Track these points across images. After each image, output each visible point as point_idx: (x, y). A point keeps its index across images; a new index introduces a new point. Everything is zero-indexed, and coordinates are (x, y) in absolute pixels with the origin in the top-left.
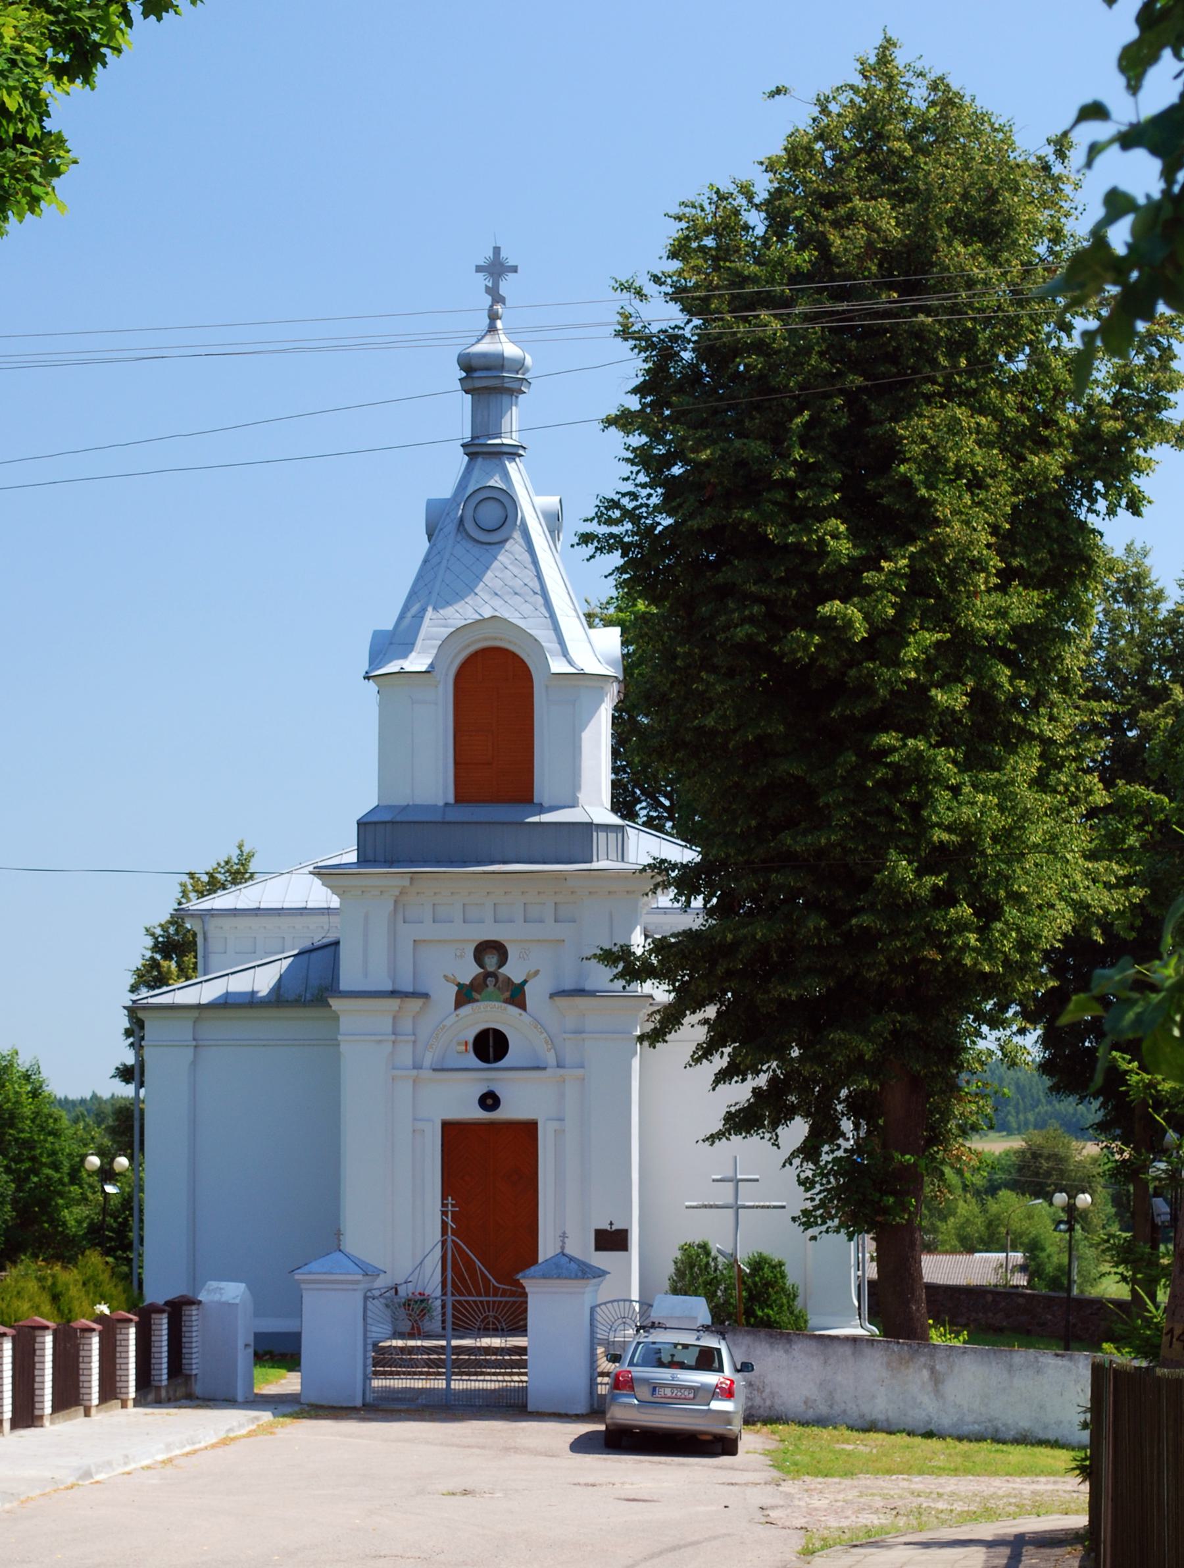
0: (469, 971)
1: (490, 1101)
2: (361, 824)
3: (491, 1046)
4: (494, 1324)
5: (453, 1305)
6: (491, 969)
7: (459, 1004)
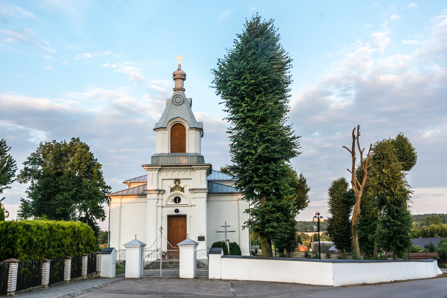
0: (173, 185)
1: (177, 211)
6: (177, 184)
7: (171, 192)
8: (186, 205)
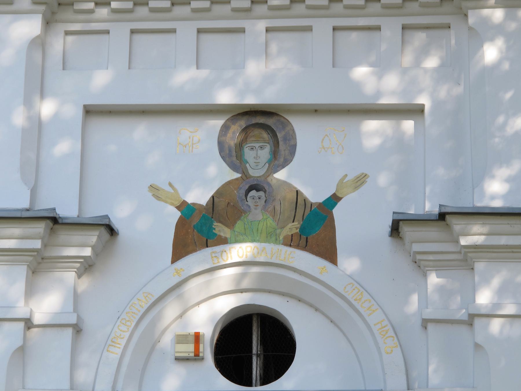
0: (205, 180)
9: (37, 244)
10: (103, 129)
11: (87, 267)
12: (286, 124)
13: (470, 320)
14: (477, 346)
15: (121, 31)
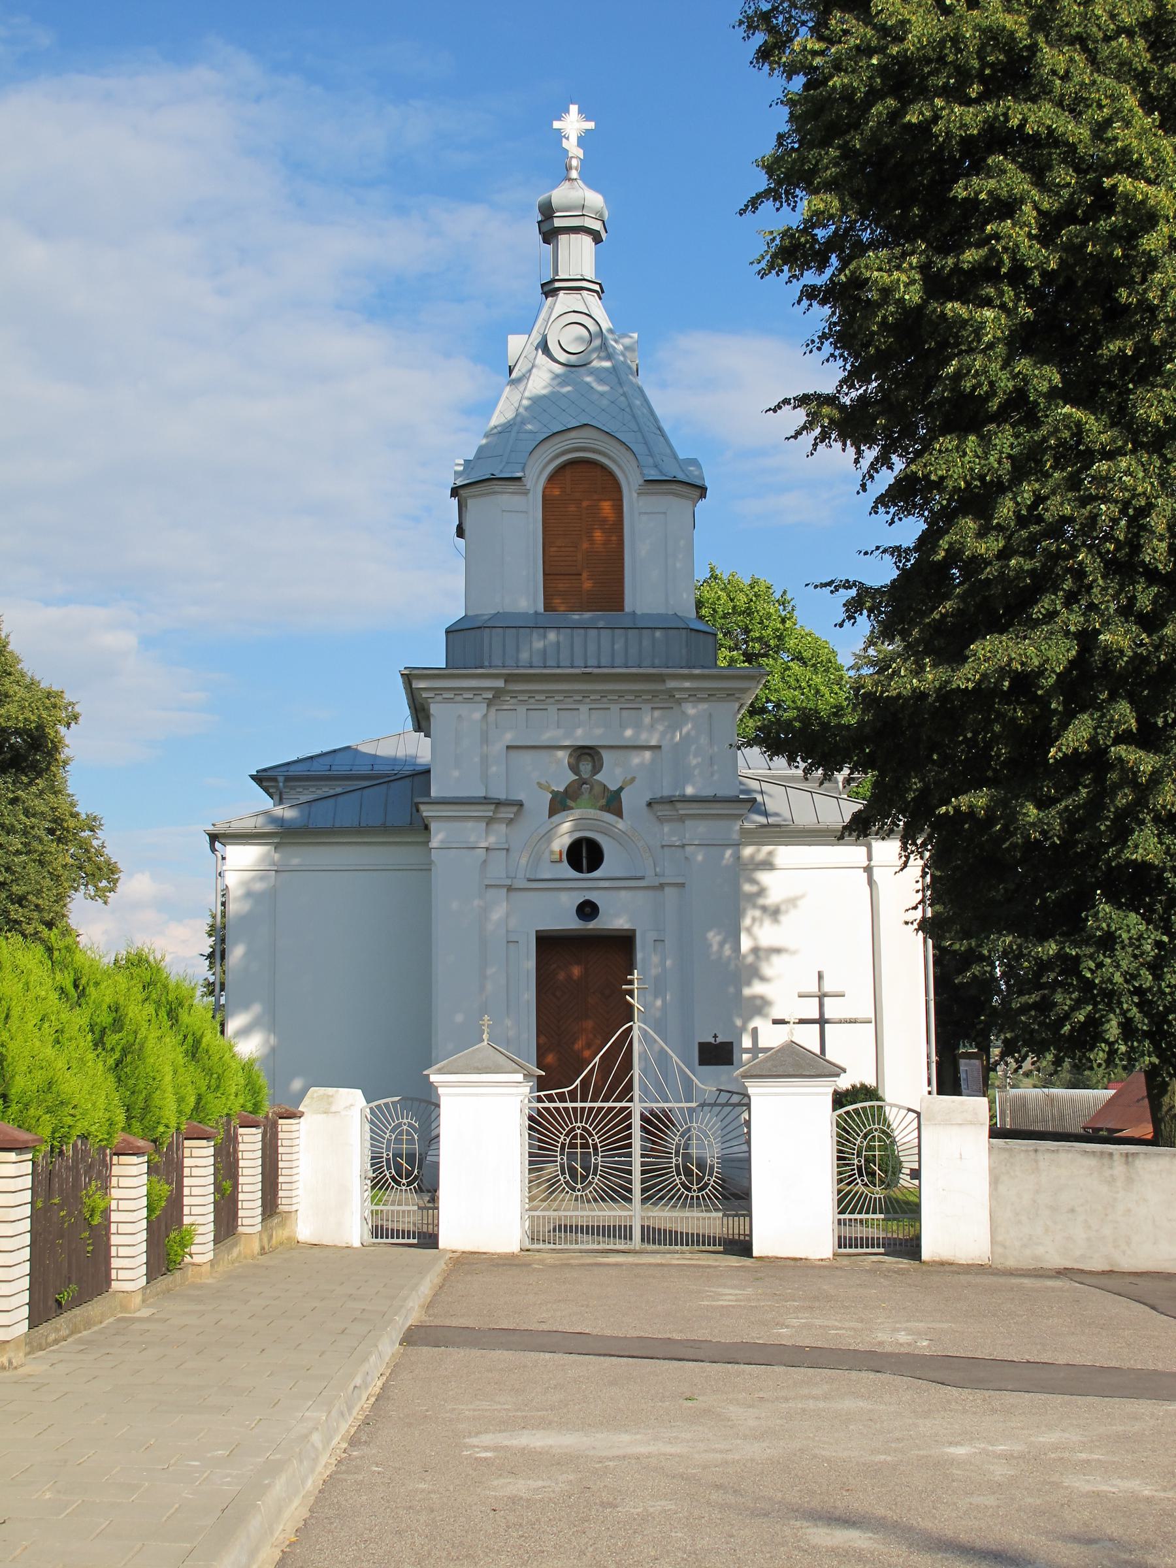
0: (563, 779)
1: (587, 910)
2: (448, 632)
3: (584, 855)
4: (583, 1137)
5: (642, 1114)
8: (631, 882)
9: (491, 814)
10: (514, 754)
11: (510, 822)
12: (599, 753)
13: (683, 846)
14: (686, 858)
15: (522, 709)
